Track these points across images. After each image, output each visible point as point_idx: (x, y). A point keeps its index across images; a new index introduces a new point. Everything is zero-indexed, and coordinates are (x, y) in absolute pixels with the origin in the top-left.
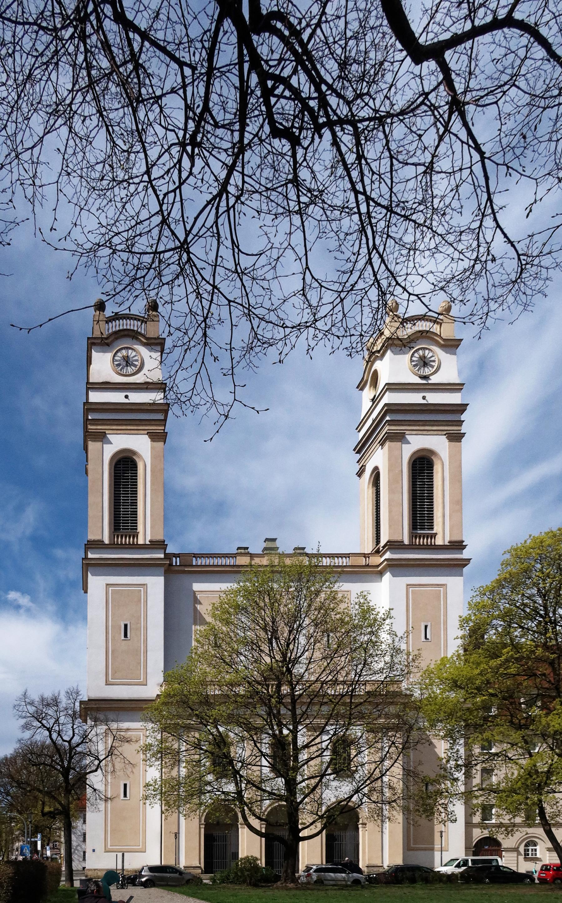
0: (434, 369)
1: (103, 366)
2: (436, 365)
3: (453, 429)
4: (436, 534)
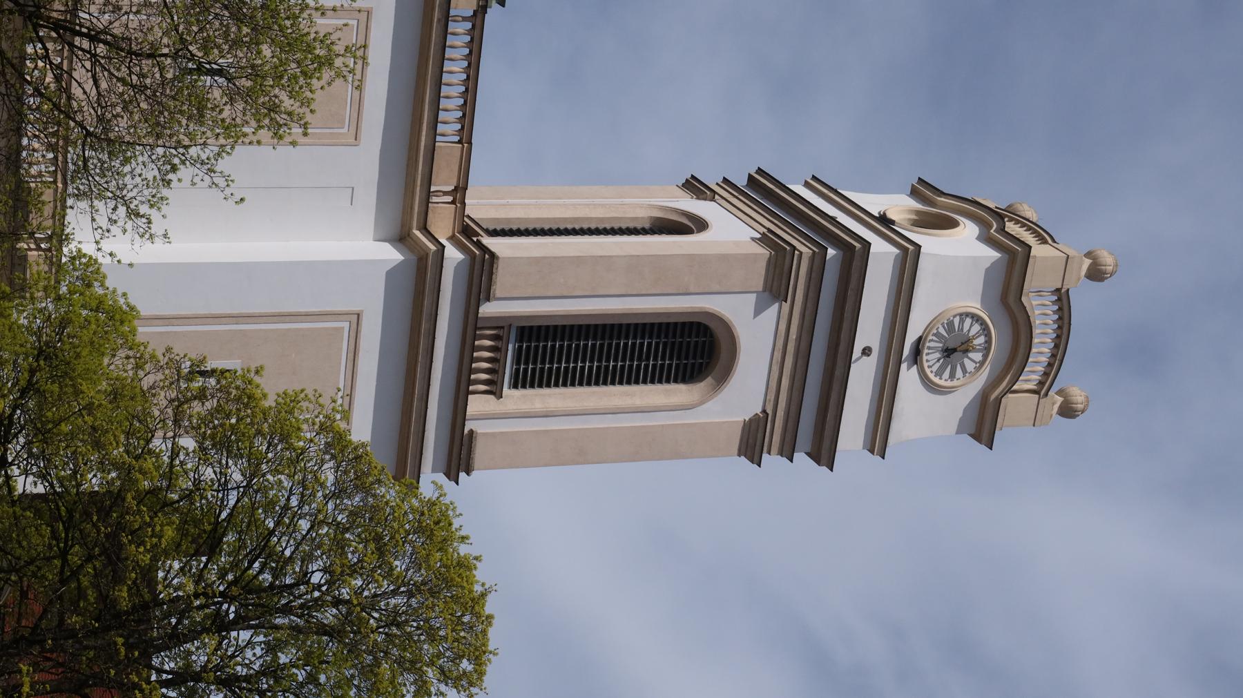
0: (932, 376)
4: (498, 395)
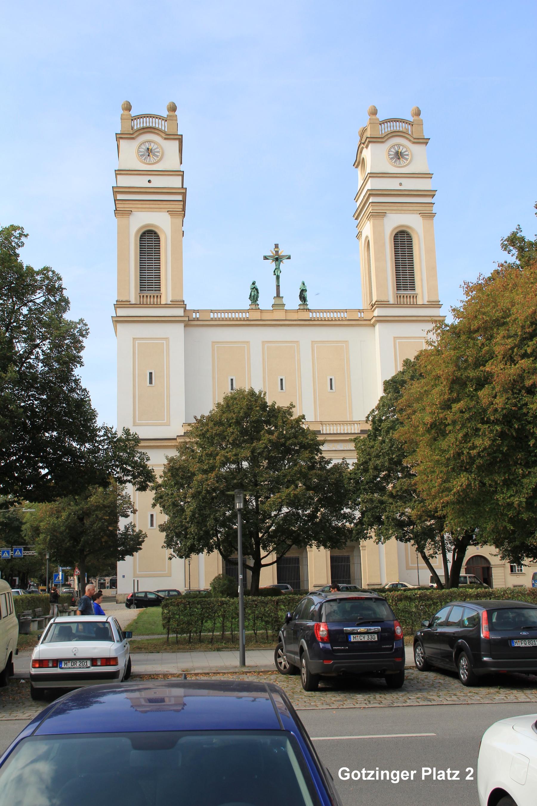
0: (408, 162)
2: (160, 155)
3: (426, 209)
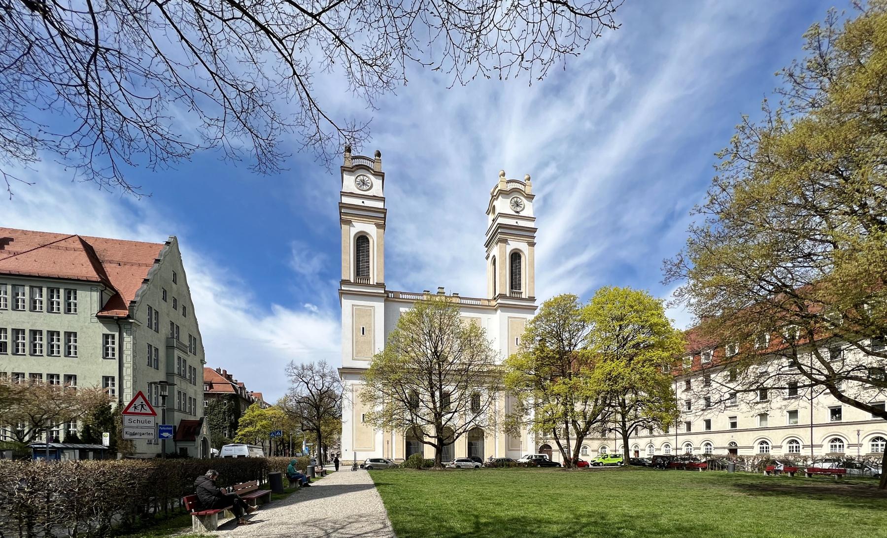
1: (350, 183)
